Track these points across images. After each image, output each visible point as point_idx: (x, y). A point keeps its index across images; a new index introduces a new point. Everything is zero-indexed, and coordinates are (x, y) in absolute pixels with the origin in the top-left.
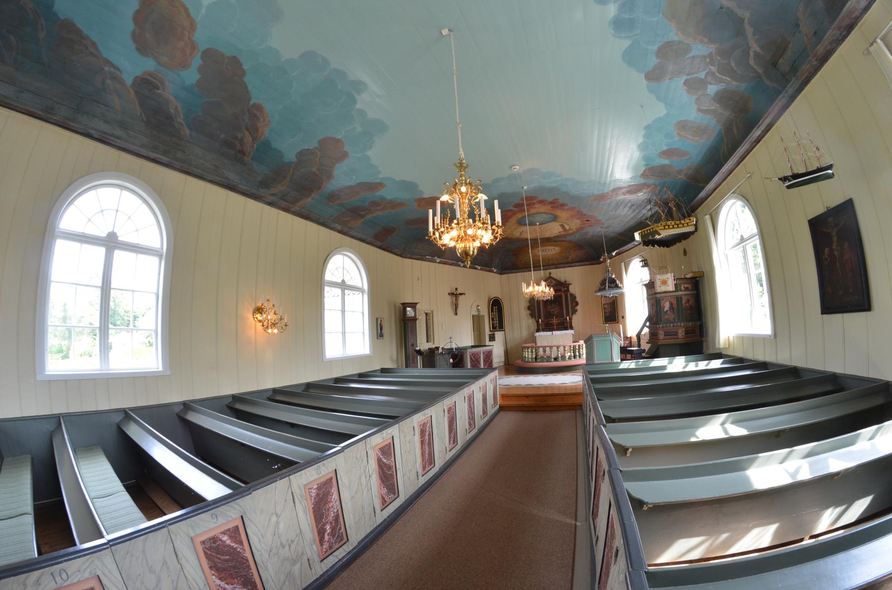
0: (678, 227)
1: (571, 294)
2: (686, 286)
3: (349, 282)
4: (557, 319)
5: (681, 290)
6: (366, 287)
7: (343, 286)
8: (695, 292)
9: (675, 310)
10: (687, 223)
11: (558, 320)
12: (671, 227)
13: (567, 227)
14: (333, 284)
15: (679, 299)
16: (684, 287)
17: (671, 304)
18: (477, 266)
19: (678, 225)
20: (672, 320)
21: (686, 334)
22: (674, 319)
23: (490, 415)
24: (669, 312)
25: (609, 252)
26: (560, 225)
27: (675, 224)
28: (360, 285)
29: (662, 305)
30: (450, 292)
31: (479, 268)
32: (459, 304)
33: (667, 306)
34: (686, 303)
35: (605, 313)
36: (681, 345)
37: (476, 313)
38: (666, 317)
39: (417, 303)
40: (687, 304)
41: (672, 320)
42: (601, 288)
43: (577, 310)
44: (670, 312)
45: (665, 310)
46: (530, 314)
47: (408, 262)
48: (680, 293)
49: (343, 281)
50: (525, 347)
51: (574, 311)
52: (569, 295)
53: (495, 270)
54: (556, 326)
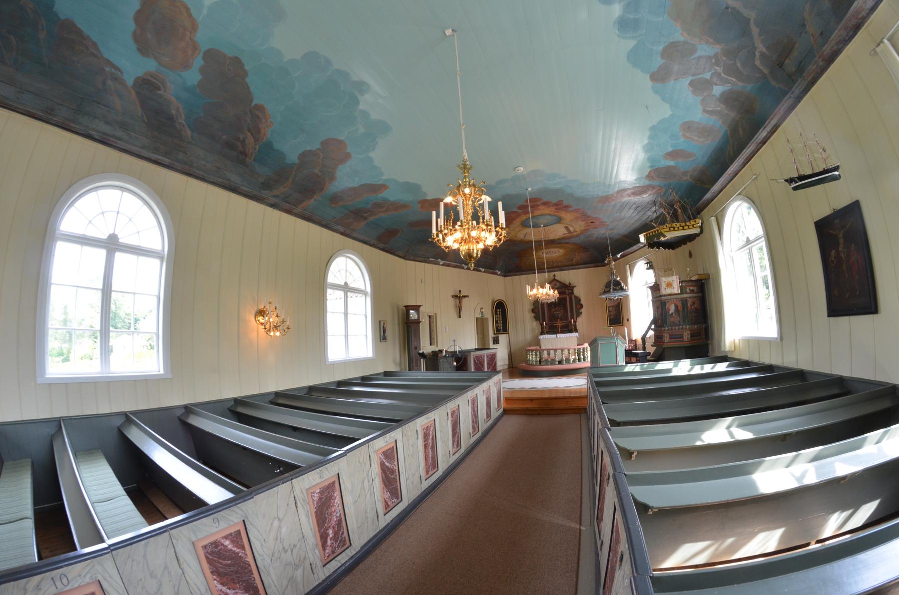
0: (683, 229)
1: (575, 296)
2: (691, 288)
3: (352, 285)
4: (561, 322)
5: (686, 293)
6: (369, 289)
7: (346, 288)
8: (701, 294)
9: (681, 313)
10: (693, 225)
11: (563, 323)
12: (676, 229)
13: (572, 229)
14: (336, 287)
15: (684, 301)
16: (690, 289)
17: (676, 307)
18: (481, 269)
19: (683, 227)
20: (677, 322)
21: (691, 337)
22: (679, 322)
24: (674, 315)
25: (614, 254)
26: (564, 227)
27: (681, 226)
28: (363, 288)
29: (667, 307)
30: (453, 294)
31: (483, 270)
32: (462, 307)
33: (672, 309)
34: (691, 306)
35: (610, 316)
36: (686, 348)
37: (479, 316)
38: (672, 319)
39: (420, 306)
40: (693, 307)
41: (677, 322)
42: (606, 290)
43: (581, 313)
44: (675, 315)
45: (670, 313)
46: (534, 317)
47: (411, 264)
48: (685, 296)
49: (346, 283)
51: (579, 314)
52: (573, 298)
53: (499, 273)
54: (561, 328)
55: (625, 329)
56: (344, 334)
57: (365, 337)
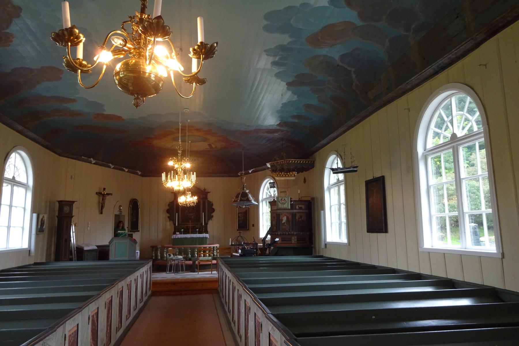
0: (285, 176)
1: (208, 201)
2: (300, 206)
3: (17, 179)
4: (192, 223)
5: (296, 209)
6: (31, 183)
7: (13, 182)
8: (307, 211)
9: (291, 223)
10: (291, 175)
11: (193, 224)
12: (281, 175)
13: (213, 146)
14: (8, 180)
15: (294, 215)
16: (299, 207)
17: (287, 218)
18: (124, 169)
19: (285, 175)
21: (298, 240)
22: (289, 229)
23: (149, 295)
24: (285, 224)
25: (247, 169)
26: (208, 145)
27: (284, 174)
28: (24, 181)
30: (98, 191)
31: (127, 170)
32: (105, 204)
33: (284, 219)
34: (299, 218)
35: (239, 221)
36: (294, 248)
37: (118, 213)
39: (74, 202)
40: (300, 219)
43: (212, 216)
44: (287, 224)
45: (283, 222)
46: (169, 217)
47: (64, 159)
48: (295, 211)
49: (14, 177)
50: (165, 247)
51: (211, 217)
52: (206, 202)
53: (140, 173)
54: (191, 229)
55: (289, 337)
56: (7, 225)
57: (21, 230)
